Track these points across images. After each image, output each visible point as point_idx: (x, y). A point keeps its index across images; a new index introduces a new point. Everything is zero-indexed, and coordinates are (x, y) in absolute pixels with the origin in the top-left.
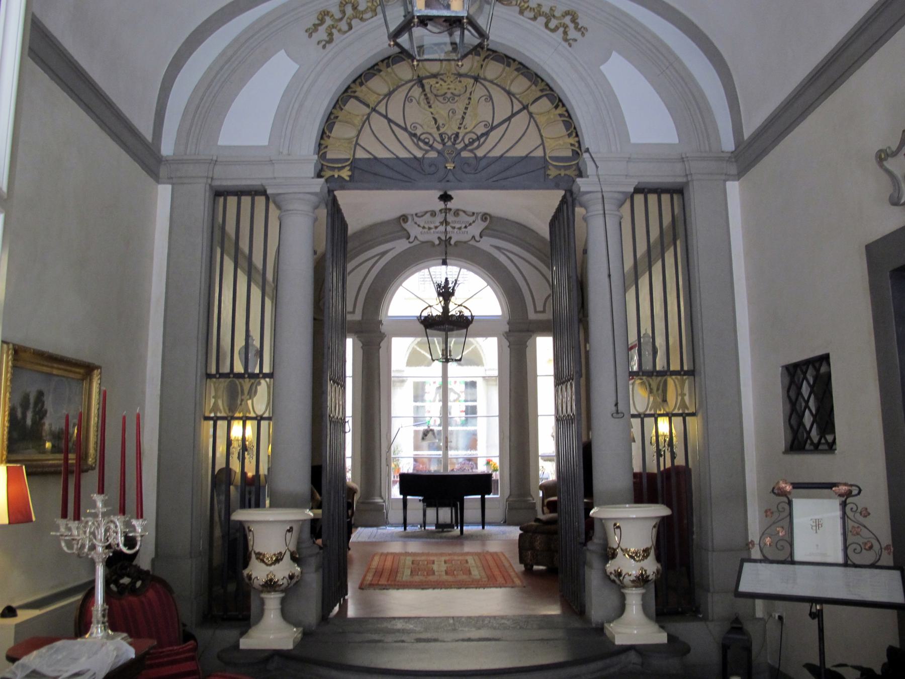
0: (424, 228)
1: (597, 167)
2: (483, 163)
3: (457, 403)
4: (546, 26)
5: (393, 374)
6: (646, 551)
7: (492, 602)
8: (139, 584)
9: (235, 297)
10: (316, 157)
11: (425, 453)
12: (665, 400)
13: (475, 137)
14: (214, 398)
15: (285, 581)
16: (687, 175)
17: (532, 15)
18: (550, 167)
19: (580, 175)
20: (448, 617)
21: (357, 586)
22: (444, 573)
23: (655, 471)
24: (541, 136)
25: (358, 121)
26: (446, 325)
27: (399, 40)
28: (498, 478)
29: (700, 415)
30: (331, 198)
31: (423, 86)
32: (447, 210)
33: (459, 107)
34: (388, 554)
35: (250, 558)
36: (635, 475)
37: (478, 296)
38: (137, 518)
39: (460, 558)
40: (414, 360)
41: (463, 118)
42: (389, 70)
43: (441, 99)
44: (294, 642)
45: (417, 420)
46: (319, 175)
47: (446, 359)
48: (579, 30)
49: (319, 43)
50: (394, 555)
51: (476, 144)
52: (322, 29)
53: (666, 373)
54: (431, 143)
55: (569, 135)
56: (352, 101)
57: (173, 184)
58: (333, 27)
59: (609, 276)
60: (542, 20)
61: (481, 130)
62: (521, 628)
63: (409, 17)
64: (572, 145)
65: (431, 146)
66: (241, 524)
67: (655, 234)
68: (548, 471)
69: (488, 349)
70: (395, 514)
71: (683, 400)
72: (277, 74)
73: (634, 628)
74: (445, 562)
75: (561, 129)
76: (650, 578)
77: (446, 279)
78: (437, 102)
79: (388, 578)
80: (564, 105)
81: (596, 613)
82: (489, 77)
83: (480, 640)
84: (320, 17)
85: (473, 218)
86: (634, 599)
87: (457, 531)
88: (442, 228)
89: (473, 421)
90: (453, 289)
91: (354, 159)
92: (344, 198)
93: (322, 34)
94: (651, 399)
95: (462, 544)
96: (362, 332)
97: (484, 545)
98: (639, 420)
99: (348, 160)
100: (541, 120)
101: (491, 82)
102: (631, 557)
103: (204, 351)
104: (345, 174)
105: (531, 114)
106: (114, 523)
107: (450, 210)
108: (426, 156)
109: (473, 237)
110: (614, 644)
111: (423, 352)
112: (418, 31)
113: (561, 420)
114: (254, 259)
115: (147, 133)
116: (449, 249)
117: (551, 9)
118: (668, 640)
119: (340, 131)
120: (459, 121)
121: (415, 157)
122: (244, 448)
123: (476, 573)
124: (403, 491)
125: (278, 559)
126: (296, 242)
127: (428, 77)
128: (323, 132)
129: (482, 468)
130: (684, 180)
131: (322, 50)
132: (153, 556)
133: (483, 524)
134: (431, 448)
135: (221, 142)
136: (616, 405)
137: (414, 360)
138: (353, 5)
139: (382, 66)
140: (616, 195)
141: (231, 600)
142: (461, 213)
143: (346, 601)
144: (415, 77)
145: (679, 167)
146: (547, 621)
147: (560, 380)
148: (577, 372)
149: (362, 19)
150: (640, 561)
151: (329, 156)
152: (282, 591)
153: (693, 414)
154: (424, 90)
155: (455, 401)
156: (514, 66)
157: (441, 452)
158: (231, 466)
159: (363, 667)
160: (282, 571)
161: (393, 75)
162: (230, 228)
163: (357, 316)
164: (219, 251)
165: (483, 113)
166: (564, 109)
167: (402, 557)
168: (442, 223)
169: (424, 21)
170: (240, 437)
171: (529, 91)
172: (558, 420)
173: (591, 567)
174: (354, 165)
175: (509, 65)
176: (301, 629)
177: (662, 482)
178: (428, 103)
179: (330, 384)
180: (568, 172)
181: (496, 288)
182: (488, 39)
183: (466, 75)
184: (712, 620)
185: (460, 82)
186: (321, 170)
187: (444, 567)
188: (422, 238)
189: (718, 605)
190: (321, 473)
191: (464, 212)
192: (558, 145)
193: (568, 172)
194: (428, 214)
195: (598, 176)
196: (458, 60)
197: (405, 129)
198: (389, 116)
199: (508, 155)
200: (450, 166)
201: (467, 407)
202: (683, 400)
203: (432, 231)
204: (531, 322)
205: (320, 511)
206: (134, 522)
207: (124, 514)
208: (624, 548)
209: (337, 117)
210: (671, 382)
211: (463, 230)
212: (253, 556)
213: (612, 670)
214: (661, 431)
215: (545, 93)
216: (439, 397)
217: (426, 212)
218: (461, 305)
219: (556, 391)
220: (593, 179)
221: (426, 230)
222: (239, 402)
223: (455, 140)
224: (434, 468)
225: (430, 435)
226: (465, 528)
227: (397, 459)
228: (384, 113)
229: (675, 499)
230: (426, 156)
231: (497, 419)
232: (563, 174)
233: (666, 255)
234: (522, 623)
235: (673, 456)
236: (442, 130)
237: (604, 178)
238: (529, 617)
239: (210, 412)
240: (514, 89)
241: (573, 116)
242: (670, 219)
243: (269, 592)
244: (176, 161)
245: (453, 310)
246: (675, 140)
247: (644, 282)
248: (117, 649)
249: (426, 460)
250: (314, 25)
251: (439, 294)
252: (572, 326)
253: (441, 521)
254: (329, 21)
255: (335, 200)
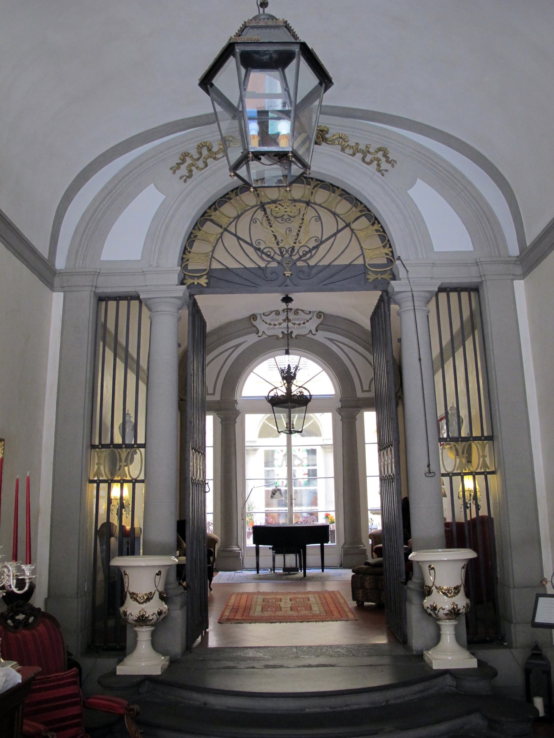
0: (270, 324)
1: (407, 271)
2: (314, 271)
3: (300, 467)
4: (363, 160)
5: (246, 444)
6: (457, 588)
7: (331, 633)
8: (31, 619)
9: (114, 381)
10: (179, 268)
11: (275, 509)
12: (469, 461)
13: (307, 249)
14: (99, 465)
15: (154, 617)
16: (481, 276)
17: (351, 152)
18: (369, 273)
19: (394, 278)
20: (293, 647)
21: (217, 621)
22: (289, 609)
23: (463, 520)
24: (361, 248)
25: (213, 239)
26: (290, 403)
27: (238, 172)
28: (335, 529)
29: (499, 473)
30: (192, 301)
31: (265, 210)
32: (288, 310)
33: (295, 225)
34: (242, 594)
35: (126, 597)
36: (447, 525)
37: (316, 379)
38: (26, 564)
39: (303, 596)
40: (264, 433)
41: (298, 235)
42: (238, 198)
43: (279, 220)
44: (162, 668)
45: (268, 483)
46: (182, 283)
47: (290, 431)
48: (390, 162)
49: (181, 178)
50: (248, 594)
51: (309, 255)
52: (184, 167)
53: (470, 439)
54: (272, 255)
55: (384, 247)
56: (208, 223)
57: (64, 292)
58: (193, 165)
59: (420, 359)
60: (359, 155)
61: (312, 244)
62: (353, 655)
63: (245, 153)
64: (386, 254)
65: (272, 258)
66: (118, 568)
67: (457, 326)
68: (375, 523)
69: (325, 422)
70: (249, 560)
71: (484, 461)
72: (147, 203)
73: (449, 654)
74: (291, 600)
75: (378, 242)
76: (461, 612)
77: (289, 366)
78: (276, 222)
79: (242, 614)
80: (379, 223)
81: (417, 641)
82: (318, 202)
83: (318, 666)
84: (182, 158)
85: (310, 316)
86: (448, 630)
87: (301, 573)
88: (285, 325)
89: (314, 482)
90: (295, 374)
91: (210, 269)
92: (202, 300)
93: (183, 171)
94: (458, 460)
95: (305, 585)
96: (221, 410)
97: (323, 585)
98: (448, 478)
99: (205, 270)
100: (360, 234)
101: (320, 205)
102: (445, 594)
103: (89, 425)
104: (203, 281)
105: (352, 230)
106: (8, 568)
107: (291, 309)
108: (268, 266)
109: (311, 331)
110: (431, 668)
111: (273, 426)
112: (254, 164)
113: (384, 480)
114: (130, 349)
115: (45, 252)
116: (291, 341)
117: (367, 147)
118: (478, 665)
119: (198, 247)
120: (294, 237)
121: (260, 267)
122: (122, 506)
123: (316, 609)
124: (256, 541)
125: (149, 598)
126: (163, 337)
127: (269, 203)
128: (185, 249)
129: (321, 521)
130: (479, 280)
131: (184, 184)
132: (46, 596)
133: (323, 567)
134: (280, 504)
135: (103, 258)
136: (429, 466)
137: (264, 433)
138: (208, 148)
139: (232, 195)
140: (423, 294)
141: (110, 631)
142: (300, 312)
143: (207, 633)
144: (259, 203)
145: (474, 269)
146: (375, 650)
147: (382, 447)
148: (395, 440)
149: (215, 159)
150: (452, 597)
151: (190, 268)
152: (152, 625)
153: (493, 473)
154: (266, 213)
155: (299, 465)
156: (338, 192)
157: (287, 508)
158: (111, 521)
159: (217, 690)
160: (152, 608)
161: (241, 202)
162: (111, 326)
163: (217, 397)
164: (101, 344)
165: (313, 231)
166: (380, 225)
167: (255, 596)
168: (284, 321)
169: (257, 156)
170: (118, 496)
171: (351, 212)
172: (382, 479)
173: (411, 602)
174: (210, 274)
175: (334, 192)
176: (168, 657)
177: (469, 530)
178: (270, 223)
179: (191, 452)
180: (384, 276)
181: (331, 373)
182: (310, 169)
183: (299, 201)
184: (516, 648)
185: (295, 206)
186: (184, 279)
187: (289, 605)
188: (269, 333)
189: (520, 634)
190: (186, 526)
191: (302, 311)
192: (376, 255)
193: (384, 276)
194: (274, 313)
195: (408, 278)
196: (286, 187)
197: (251, 245)
198: (238, 234)
199: (335, 263)
200: (288, 273)
201: (309, 470)
202: (484, 461)
203: (276, 327)
204: (359, 399)
205: (184, 558)
206: (24, 567)
207: (16, 561)
208: (438, 586)
209: (196, 236)
210: (475, 447)
211: (302, 325)
212: (128, 596)
213: (431, 692)
214: (466, 488)
215: (363, 213)
216: (285, 463)
217: (272, 312)
218: (301, 387)
219: (380, 455)
220: (404, 281)
221: (272, 326)
222: (118, 468)
223: (292, 253)
224: (282, 522)
225: (277, 494)
226: (307, 571)
227: (251, 514)
228: (234, 233)
229: (480, 543)
230: (268, 266)
231: (333, 480)
232: (379, 277)
233: (466, 342)
234: (353, 651)
235: (478, 508)
236: (281, 245)
237: (413, 280)
238: (360, 646)
239: (94, 477)
240: (338, 211)
241: (387, 231)
242: (469, 313)
243: (141, 626)
244: (68, 273)
245: (295, 390)
246: (471, 248)
247: (449, 366)
248: (7, 675)
249: (276, 515)
250: (177, 164)
251: (284, 378)
252: (391, 400)
253: (288, 565)
254: (189, 161)
255: (195, 303)
